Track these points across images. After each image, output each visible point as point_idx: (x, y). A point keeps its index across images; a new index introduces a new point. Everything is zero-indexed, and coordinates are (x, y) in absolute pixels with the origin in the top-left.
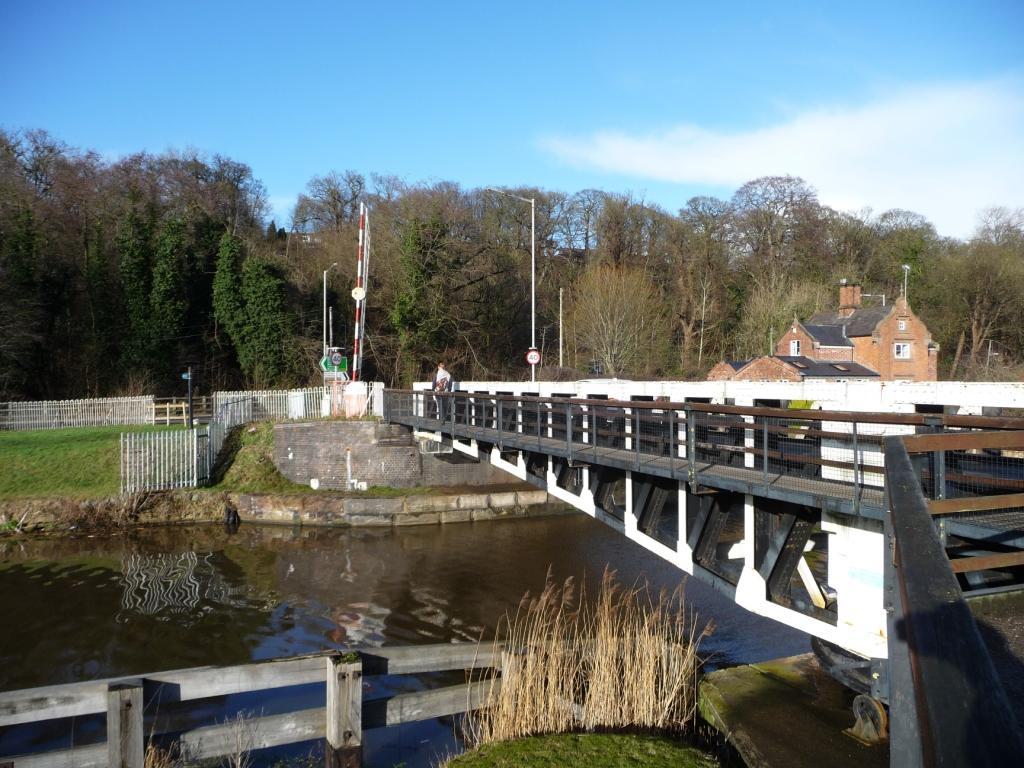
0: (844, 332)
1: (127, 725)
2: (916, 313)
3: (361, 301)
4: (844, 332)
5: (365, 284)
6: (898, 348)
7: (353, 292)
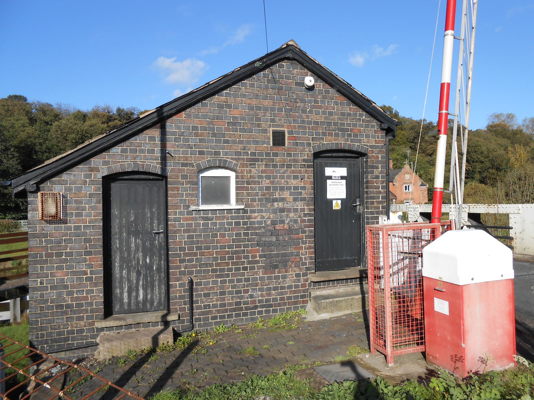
6: (406, 187)
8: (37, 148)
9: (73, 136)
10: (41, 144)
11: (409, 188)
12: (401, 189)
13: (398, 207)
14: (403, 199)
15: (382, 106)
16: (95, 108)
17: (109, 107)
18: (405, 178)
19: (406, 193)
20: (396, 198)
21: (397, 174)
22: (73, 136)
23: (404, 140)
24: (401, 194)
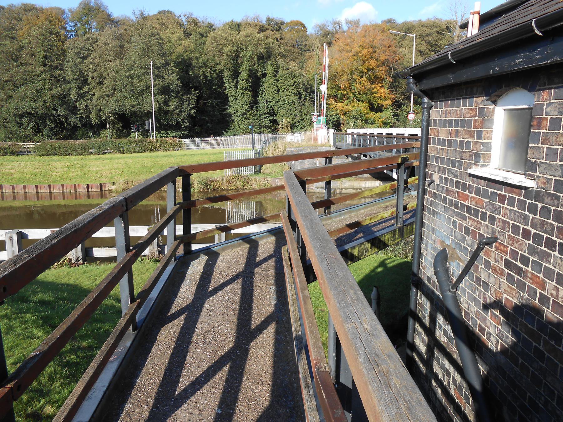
5: (326, 82)
10: (197, 58)
22: (229, 48)
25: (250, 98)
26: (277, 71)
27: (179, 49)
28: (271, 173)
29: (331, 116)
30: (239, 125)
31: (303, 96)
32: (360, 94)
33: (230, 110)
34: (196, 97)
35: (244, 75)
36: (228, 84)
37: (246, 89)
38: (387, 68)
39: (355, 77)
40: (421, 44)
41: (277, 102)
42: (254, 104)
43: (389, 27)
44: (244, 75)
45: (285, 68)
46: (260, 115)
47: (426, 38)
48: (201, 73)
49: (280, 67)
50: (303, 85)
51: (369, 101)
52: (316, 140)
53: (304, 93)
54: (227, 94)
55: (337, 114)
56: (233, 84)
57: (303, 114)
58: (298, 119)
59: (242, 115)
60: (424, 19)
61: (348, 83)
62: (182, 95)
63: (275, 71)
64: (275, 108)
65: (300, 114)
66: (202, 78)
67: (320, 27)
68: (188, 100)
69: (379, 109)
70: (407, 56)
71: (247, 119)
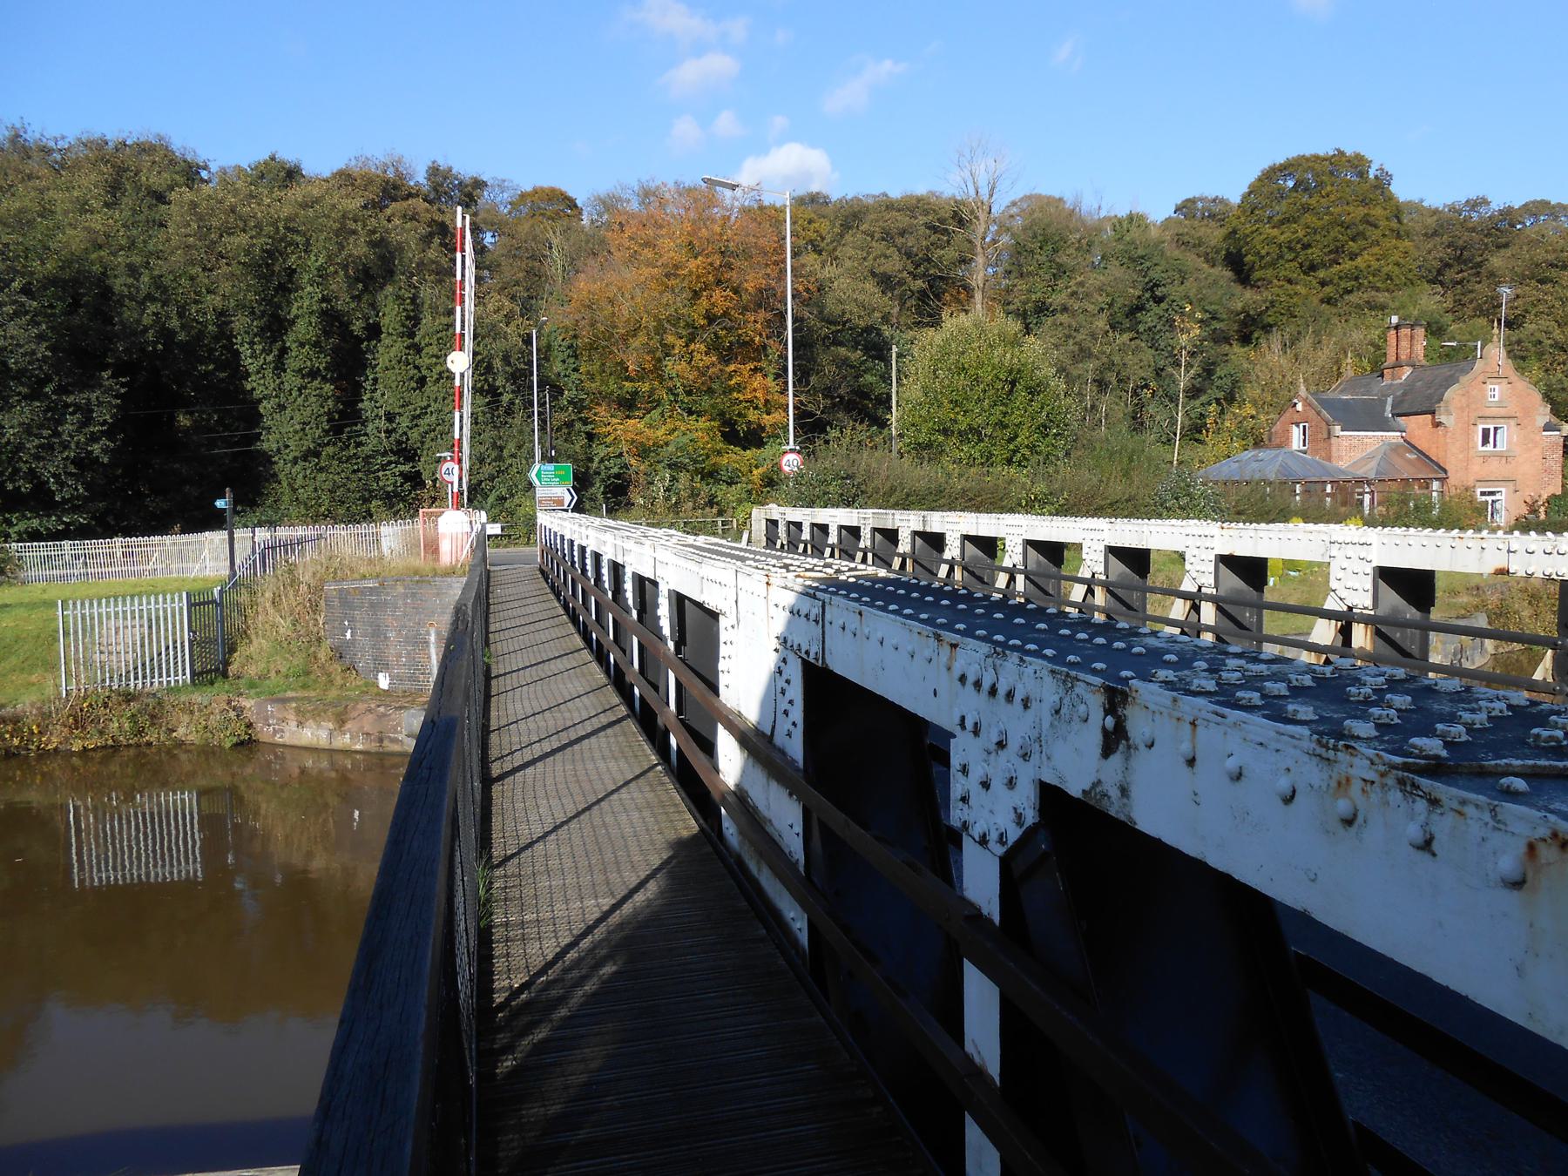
0: (1389, 408)
1: (640, 591)
2: (1520, 370)
3: (462, 375)
4: (1389, 408)
5: (469, 343)
6: (1486, 433)
7: (449, 358)
8: (119, 284)
9: (242, 239)
10: (133, 271)
11: (1498, 436)
12: (1467, 446)
13: (891, 517)
14: (1471, 483)
15: (1331, 153)
16: (353, 163)
17: (399, 161)
18: (1484, 397)
19: (1486, 457)
20: (1443, 475)
21: (1450, 381)
22: (242, 239)
23: (1410, 271)
24: (1468, 460)
25: (330, 402)
26: (416, 320)
27: (73, 239)
28: (263, 677)
29: (602, 461)
30: (294, 490)
31: (506, 398)
32: (689, 393)
33: (268, 444)
34: (116, 397)
35: (304, 328)
36: (251, 358)
37: (313, 374)
38: (769, 316)
39: (670, 339)
40: (886, 257)
41: (419, 417)
42: (345, 419)
43: (813, 215)
44: (304, 328)
45: (441, 310)
46: (367, 459)
47: (899, 241)
48: (147, 320)
49: (426, 306)
50: (506, 359)
51: (722, 414)
52: (433, 547)
53: (509, 387)
54: (253, 389)
55: (621, 455)
56: (270, 358)
57: (506, 453)
58: (487, 470)
59: (305, 458)
60: (895, 193)
61: (649, 358)
62: (62, 390)
63: (408, 318)
64: (414, 435)
65: (494, 454)
66: (150, 335)
67: (604, 203)
68: (86, 412)
69: (754, 438)
70: (836, 283)
71: (321, 470)
